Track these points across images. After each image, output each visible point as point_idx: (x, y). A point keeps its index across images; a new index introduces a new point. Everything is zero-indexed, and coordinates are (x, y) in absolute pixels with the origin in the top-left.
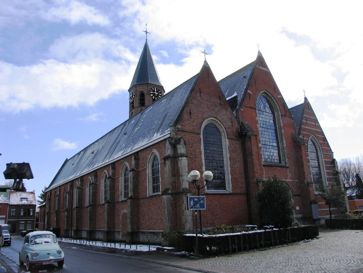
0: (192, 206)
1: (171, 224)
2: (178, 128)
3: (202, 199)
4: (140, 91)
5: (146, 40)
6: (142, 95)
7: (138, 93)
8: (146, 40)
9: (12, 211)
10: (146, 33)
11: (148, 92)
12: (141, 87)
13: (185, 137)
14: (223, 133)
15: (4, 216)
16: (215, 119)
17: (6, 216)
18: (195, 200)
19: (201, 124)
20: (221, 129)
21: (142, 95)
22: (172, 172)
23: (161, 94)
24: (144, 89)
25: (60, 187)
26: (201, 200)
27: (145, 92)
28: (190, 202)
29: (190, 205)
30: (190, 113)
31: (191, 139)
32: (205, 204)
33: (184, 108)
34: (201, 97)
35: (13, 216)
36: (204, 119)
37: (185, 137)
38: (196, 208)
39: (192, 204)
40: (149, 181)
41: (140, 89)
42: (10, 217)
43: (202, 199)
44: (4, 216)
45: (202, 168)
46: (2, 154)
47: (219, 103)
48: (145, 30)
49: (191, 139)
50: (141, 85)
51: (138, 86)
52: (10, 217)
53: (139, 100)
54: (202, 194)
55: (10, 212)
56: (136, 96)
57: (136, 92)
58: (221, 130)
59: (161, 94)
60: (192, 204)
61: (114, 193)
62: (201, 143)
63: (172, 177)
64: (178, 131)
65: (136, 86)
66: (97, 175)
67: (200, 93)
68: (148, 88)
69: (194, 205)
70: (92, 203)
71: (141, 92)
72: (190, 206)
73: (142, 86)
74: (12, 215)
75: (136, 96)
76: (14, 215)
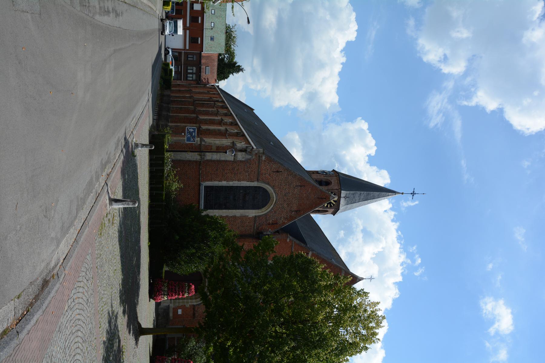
0: (189, 130)
1: (175, 142)
2: (262, 156)
3: (194, 140)
4: (332, 181)
5: (402, 193)
6: (328, 183)
7: (329, 178)
8: (402, 193)
9: (193, 56)
10: (411, 194)
11: (331, 190)
12: (336, 182)
13: (254, 164)
14: (261, 211)
15: (187, 48)
16: (274, 202)
17: (187, 50)
18: (194, 133)
19: (268, 184)
20: (265, 210)
21: (328, 183)
22: (221, 147)
23: (329, 206)
24: (334, 185)
25: (218, 94)
26: (193, 139)
27: (330, 187)
28: (192, 128)
29: (190, 128)
30: (278, 172)
31: (253, 171)
32: (190, 142)
33: (230, 38)
34: (296, 186)
35: (188, 57)
36: (273, 187)
37: (254, 164)
38: (187, 134)
39: (190, 130)
40: (215, 140)
41: (334, 180)
42: (187, 54)
43: (194, 140)
44: (187, 48)
45: (225, 181)
46: (249, 24)
47: (293, 209)
48: (415, 192)
49: (253, 171)
50: (339, 182)
51: (338, 178)
52: (187, 54)
53: (320, 180)
54: (200, 178)
55: (193, 54)
56: (325, 176)
57: (330, 176)
58: (263, 209)
59: (329, 206)
60: (190, 130)
61: (207, 124)
62: (249, 182)
63: (216, 146)
64: (259, 156)
65: (338, 176)
66: (226, 116)
67: (300, 186)
68: (336, 189)
69: (190, 132)
70: (198, 110)
71: (330, 182)
72: (189, 128)
73: (338, 183)
74: (189, 56)
75: (325, 176)
76: (189, 59)
